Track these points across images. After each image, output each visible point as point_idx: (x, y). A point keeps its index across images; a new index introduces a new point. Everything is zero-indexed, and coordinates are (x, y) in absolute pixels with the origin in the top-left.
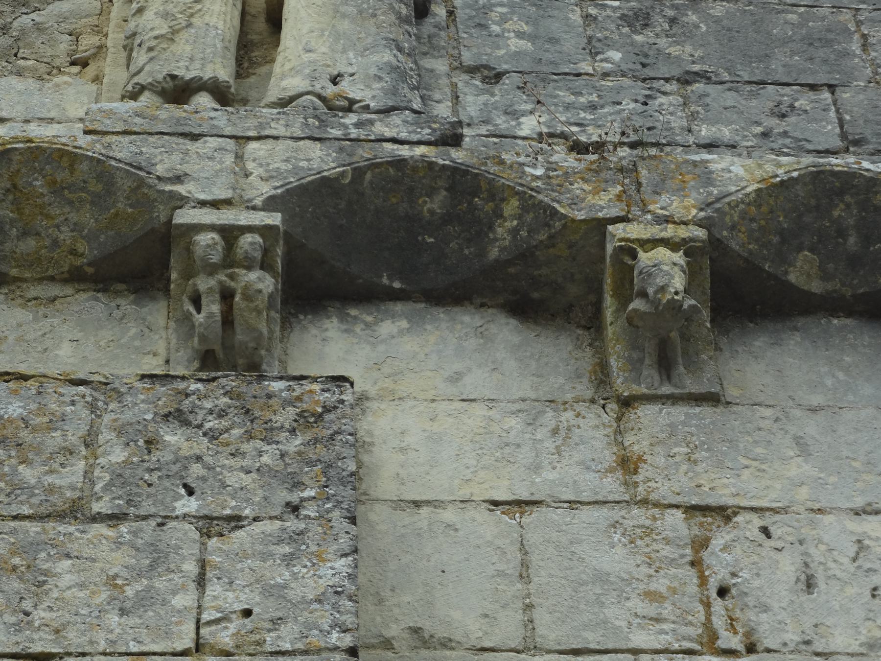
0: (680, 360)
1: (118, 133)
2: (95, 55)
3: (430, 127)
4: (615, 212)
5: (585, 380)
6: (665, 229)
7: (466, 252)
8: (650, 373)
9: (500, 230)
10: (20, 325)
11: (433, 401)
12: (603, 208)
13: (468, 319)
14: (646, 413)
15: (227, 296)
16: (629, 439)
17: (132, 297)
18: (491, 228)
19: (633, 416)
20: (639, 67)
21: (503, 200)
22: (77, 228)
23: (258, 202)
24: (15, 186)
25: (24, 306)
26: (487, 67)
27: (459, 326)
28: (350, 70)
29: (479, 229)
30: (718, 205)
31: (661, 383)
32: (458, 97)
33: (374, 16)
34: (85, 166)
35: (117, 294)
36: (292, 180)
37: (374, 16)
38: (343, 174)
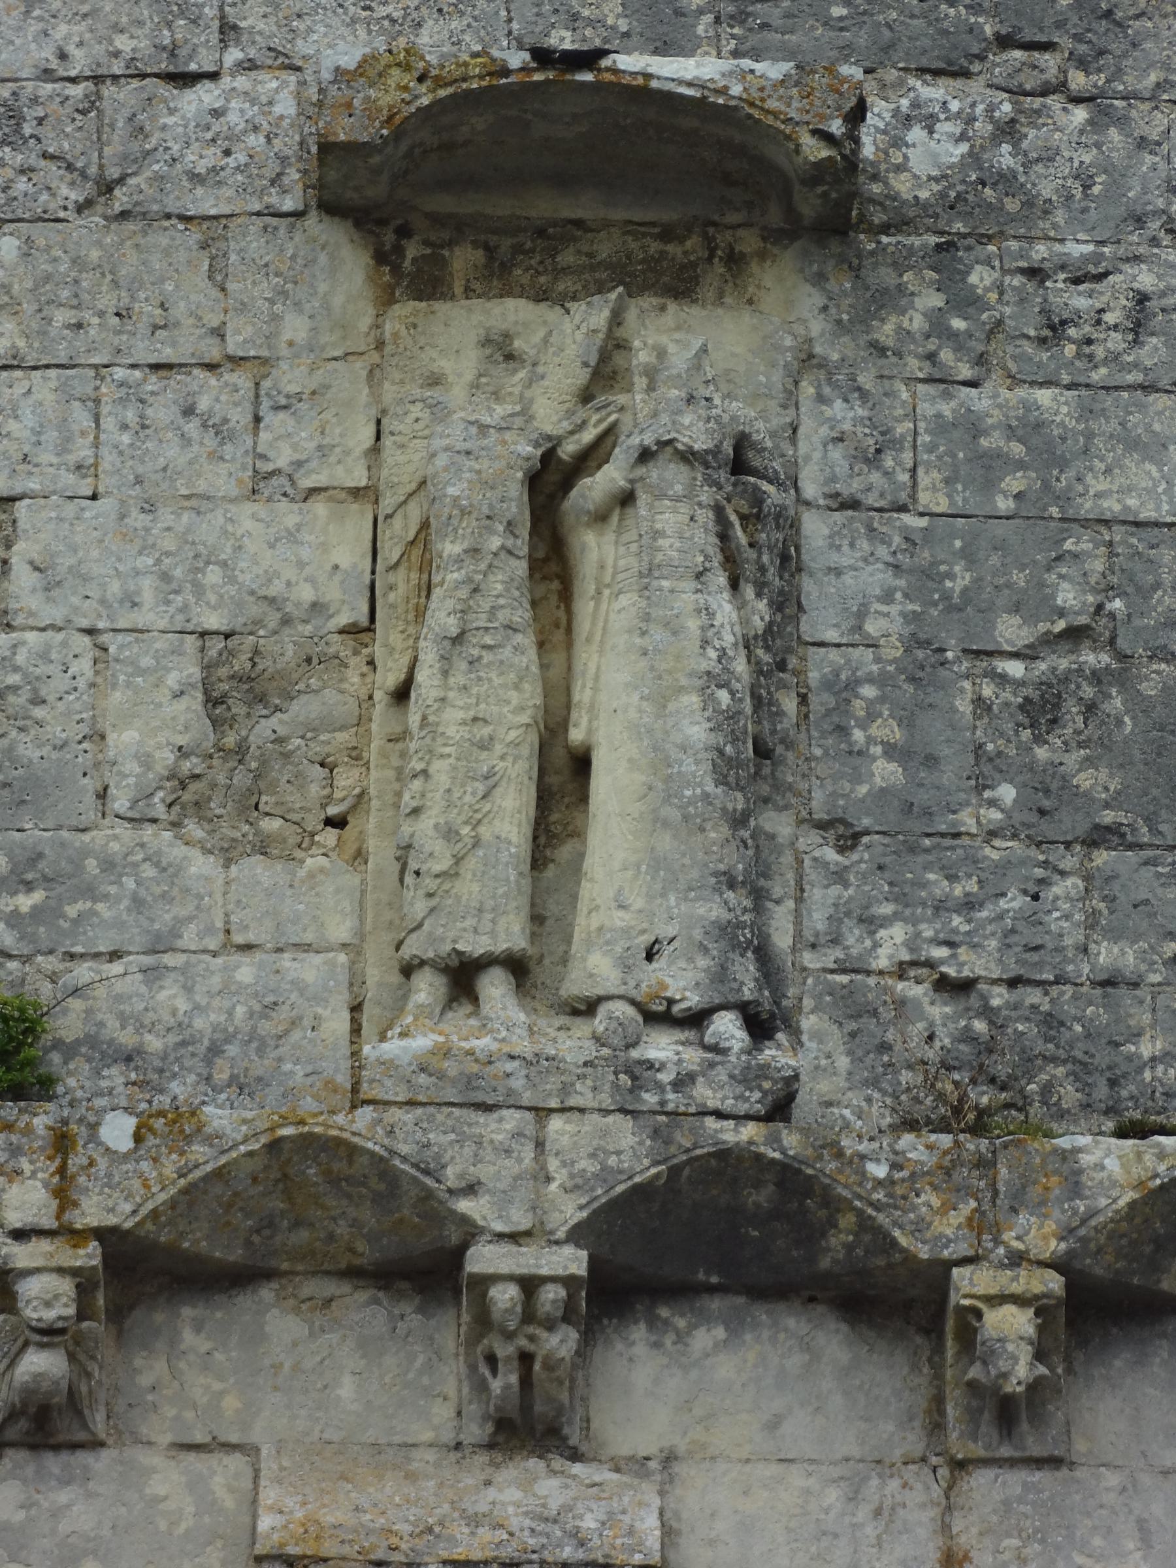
0: (1024, 1416)
1: (400, 1104)
2: (354, 807)
3: (760, 1088)
4: (963, 1249)
5: (917, 1424)
6: (1016, 1279)
7: (795, 1253)
8: (987, 1427)
9: (833, 1241)
10: (295, 1344)
11: (748, 1461)
12: (950, 1241)
13: (794, 1322)
14: (981, 1480)
15: (526, 1359)
16: (957, 1525)
17: (417, 1301)
18: (823, 1235)
19: (965, 1487)
20: (1033, 818)
21: (838, 1210)
22: (355, 1223)
23: (561, 1234)
24: (285, 1176)
25: (297, 1311)
26: (842, 821)
27: (782, 1336)
28: (671, 931)
29: (811, 1235)
30: (1082, 1232)
31: (1000, 1443)
32: (802, 890)
33: (702, 829)
34: (365, 1160)
35: (400, 1296)
36: (599, 1191)
37: (702, 829)
38: (657, 1176)
